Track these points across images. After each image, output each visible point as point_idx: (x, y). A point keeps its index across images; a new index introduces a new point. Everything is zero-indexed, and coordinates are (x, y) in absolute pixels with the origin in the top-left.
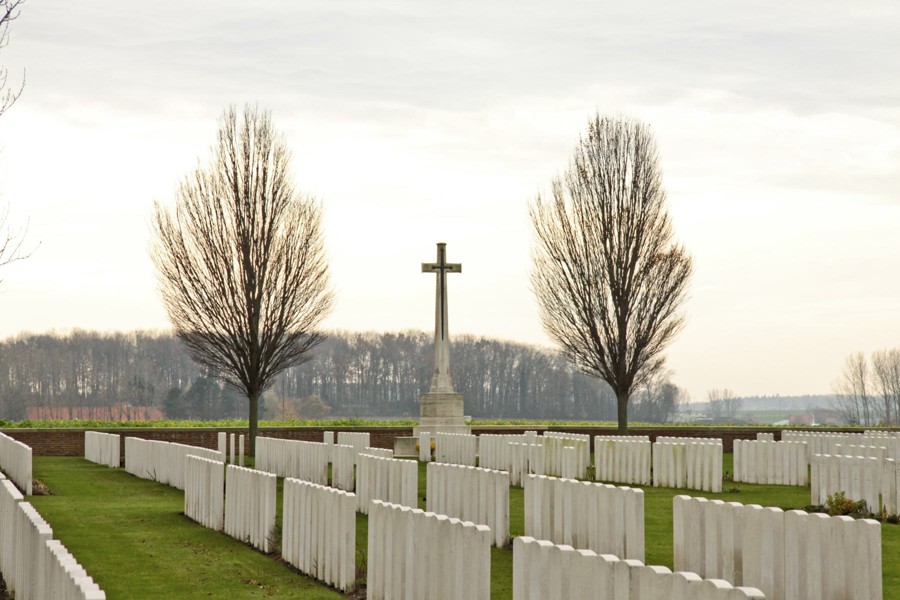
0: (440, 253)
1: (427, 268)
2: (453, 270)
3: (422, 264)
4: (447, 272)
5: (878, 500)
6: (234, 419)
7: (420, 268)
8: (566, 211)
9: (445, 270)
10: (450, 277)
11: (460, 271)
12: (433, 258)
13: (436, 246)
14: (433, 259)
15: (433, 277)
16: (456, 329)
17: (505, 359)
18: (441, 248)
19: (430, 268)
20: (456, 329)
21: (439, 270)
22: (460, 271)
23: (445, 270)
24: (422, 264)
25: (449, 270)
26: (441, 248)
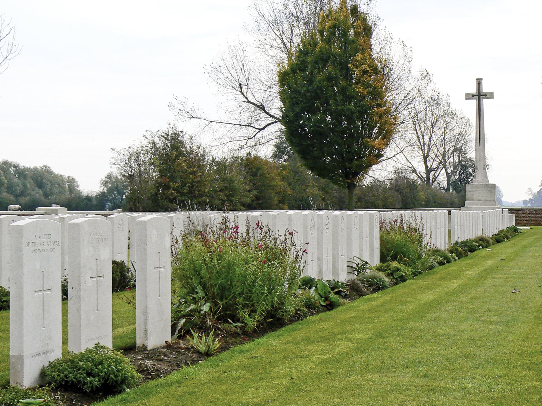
0: (478, 85)
1: (490, 96)
2: (487, 96)
3: (466, 93)
4: (483, 98)
5: (69, 323)
6: (393, 176)
7: (495, 96)
8: (127, 239)
9: (481, 97)
10: (486, 102)
11: (492, 98)
12: (474, 90)
13: (476, 80)
14: (474, 90)
15: (474, 103)
16: (446, 212)
17: (375, 139)
18: (479, 82)
19: (471, 97)
20: (446, 212)
21: (477, 97)
22: (492, 98)
23: (481, 97)
24: (466, 93)
25: (484, 96)
26: (479, 82)
